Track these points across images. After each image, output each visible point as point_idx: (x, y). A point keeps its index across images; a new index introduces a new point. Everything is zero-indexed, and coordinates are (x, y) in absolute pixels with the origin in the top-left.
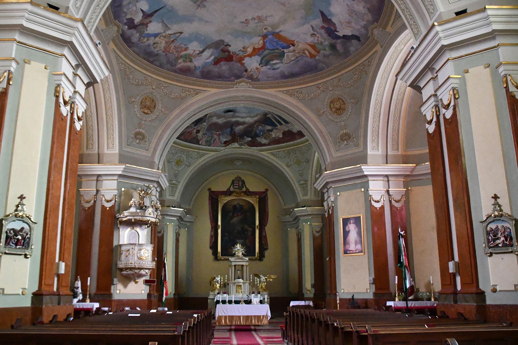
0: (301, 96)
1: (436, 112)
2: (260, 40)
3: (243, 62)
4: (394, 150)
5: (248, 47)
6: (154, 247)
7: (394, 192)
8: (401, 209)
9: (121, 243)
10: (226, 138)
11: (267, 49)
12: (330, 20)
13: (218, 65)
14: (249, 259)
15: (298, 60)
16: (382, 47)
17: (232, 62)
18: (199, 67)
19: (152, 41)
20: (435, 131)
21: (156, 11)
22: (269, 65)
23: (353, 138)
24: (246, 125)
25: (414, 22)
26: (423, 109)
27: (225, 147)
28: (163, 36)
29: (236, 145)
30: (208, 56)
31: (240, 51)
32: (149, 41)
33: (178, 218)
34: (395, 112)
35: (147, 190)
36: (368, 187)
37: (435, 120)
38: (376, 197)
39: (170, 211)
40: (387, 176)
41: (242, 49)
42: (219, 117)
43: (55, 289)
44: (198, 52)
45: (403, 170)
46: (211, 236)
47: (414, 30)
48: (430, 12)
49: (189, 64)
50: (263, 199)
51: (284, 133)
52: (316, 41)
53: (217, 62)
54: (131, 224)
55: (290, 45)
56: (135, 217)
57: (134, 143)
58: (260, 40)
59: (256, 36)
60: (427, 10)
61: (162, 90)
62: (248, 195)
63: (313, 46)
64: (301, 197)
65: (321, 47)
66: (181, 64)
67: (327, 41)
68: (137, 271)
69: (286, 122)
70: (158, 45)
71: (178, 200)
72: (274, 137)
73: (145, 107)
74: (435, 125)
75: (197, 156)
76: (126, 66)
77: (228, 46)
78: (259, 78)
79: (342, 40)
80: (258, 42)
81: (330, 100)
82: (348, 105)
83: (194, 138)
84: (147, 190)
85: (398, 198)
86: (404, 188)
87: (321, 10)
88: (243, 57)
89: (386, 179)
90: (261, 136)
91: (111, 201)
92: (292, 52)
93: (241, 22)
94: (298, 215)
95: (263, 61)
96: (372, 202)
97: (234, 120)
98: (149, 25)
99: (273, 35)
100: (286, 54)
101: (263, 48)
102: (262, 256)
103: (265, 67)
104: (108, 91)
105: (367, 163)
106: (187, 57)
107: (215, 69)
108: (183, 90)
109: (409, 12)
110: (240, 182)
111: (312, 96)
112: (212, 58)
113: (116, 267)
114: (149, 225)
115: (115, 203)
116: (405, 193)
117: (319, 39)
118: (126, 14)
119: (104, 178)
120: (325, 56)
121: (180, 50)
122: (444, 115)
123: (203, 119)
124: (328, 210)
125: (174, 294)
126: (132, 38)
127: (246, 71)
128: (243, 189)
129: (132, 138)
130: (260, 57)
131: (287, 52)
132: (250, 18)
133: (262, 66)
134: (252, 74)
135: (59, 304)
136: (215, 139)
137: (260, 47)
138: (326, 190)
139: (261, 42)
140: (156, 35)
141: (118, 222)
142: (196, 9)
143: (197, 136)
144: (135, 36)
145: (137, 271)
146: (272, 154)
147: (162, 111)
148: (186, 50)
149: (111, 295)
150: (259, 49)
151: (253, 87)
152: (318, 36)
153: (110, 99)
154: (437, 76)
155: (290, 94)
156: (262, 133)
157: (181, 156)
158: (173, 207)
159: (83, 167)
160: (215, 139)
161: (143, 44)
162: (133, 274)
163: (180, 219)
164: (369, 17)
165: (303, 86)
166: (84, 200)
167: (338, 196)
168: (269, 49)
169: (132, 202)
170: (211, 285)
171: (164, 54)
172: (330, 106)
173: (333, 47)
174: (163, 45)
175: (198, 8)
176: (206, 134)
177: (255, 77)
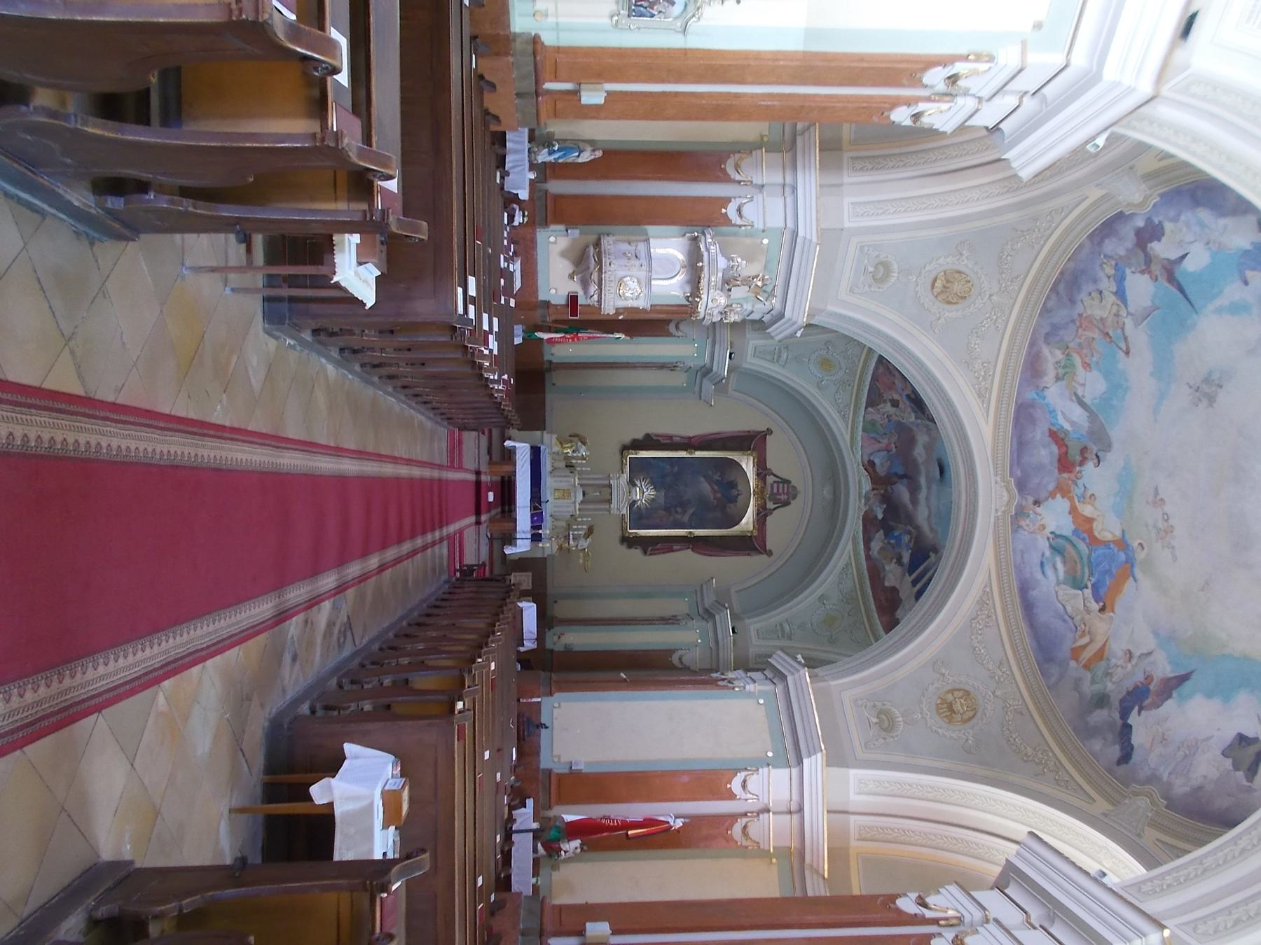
0: (980, 624)
1: (946, 919)
2: (1112, 533)
3: (1058, 496)
4: (860, 829)
5: (1093, 505)
6: (644, 310)
7: (766, 822)
8: (730, 839)
9: (651, 240)
10: (882, 464)
11: (1091, 551)
12: (1170, 696)
13: (1049, 439)
14: (623, 515)
15: (1064, 621)
16: (1105, 815)
17: (1056, 471)
18: (1044, 398)
19: (1108, 286)
20: (899, 912)
21: (1181, 290)
22: (1052, 554)
23: (885, 739)
24: (910, 507)
25: (1169, 886)
26: (953, 889)
27: (862, 462)
28: (1118, 311)
29: (867, 486)
30: (1071, 417)
31: (1085, 487)
32: (1107, 279)
33: (708, 365)
34: (946, 837)
35: (765, 291)
36: (775, 767)
37: (929, 914)
38: (754, 782)
39: (722, 348)
40: (801, 810)
41: (1089, 494)
42: (929, 448)
43: (548, 86)
44: (1080, 393)
45: (815, 855)
46: (671, 437)
47: (1149, 884)
48: (1196, 926)
49: (1051, 373)
50: (750, 545)
51: (894, 590)
52: (1114, 661)
53: (1056, 436)
54: (695, 258)
55: (1101, 601)
56: (706, 269)
57: (866, 261)
58: (1112, 533)
59: (1121, 524)
60: (1204, 919)
61: (989, 317)
62: (758, 514)
63: (1100, 654)
64: (754, 625)
65: (1100, 673)
66: (1051, 357)
67: (1115, 688)
68: (595, 276)
69: (919, 595)
70: (1096, 302)
71: (745, 365)
72: (885, 570)
73: (948, 281)
74: (916, 915)
75: (841, 403)
76: (1045, 231)
77: (1096, 461)
78: (1021, 531)
79: (1119, 722)
80: (1108, 528)
81: (968, 688)
82: (960, 731)
83: (880, 395)
84: (765, 291)
85: (752, 831)
86: (774, 848)
87: (1194, 676)
88: (1071, 495)
89: (794, 807)
90: (886, 541)
91: (740, 215)
92: (1084, 606)
93: (1156, 489)
94: (717, 617)
95: (1061, 541)
96: (743, 774)
97: (923, 480)
98: (1146, 276)
99: (1126, 562)
100: (1080, 592)
101: (1093, 541)
102: (629, 542)
103: (1048, 545)
104: (985, 195)
105: (828, 765)
106: (1067, 370)
107: (1039, 433)
108: (989, 363)
109: (1196, 876)
110: (786, 497)
111: (980, 650)
112: (1067, 426)
113: (604, 235)
114: (690, 299)
115: (735, 225)
116: (763, 850)
117: (1120, 668)
118: (1175, 220)
119: (789, 200)
120: (1077, 684)
121: (1085, 351)
122: (940, 935)
123: (924, 414)
124: (724, 680)
125: (550, 362)
126: (1114, 239)
127: (1037, 503)
128: (772, 503)
129: (877, 256)
130: (1070, 534)
131: (1086, 596)
132: (1168, 508)
133: (1048, 539)
134: (1028, 516)
135: (518, 95)
136: (879, 442)
137: (1096, 534)
138: (770, 675)
139: (1108, 537)
140: (1121, 294)
141: (696, 234)
142: (1188, 384)
143: (885, 401)
144: (1118, 247)
145: (595, 276)
146: (847, 565)
147: (939, 319)
148: (1085, 365)
149: (545, 223)
150: (1090, 532)
151: (997, 518)
152: (1126, 667)
153: (966, 200)
154: (1035, 928)
155: (984, 601)
156: (893, 541)
157: (841, 368)
158: (731, 354)
159: (813, 148)
160: (879, 442)
161: (1098, 268)
162: (589, 268)
163: (706, 371)
164: (1180, 787)
165: (1003, 629)
166: (741, 159)
167: (755, 701)
168: (1090, 555)
169: (739, 260)
170: (570, 436)
171: (1076, 317)
172: (957, 690)
173: (1101, 701)
174: (1098, 313)
175: (1190, 387)
176: (889, 421)
177: (1023, 523)
